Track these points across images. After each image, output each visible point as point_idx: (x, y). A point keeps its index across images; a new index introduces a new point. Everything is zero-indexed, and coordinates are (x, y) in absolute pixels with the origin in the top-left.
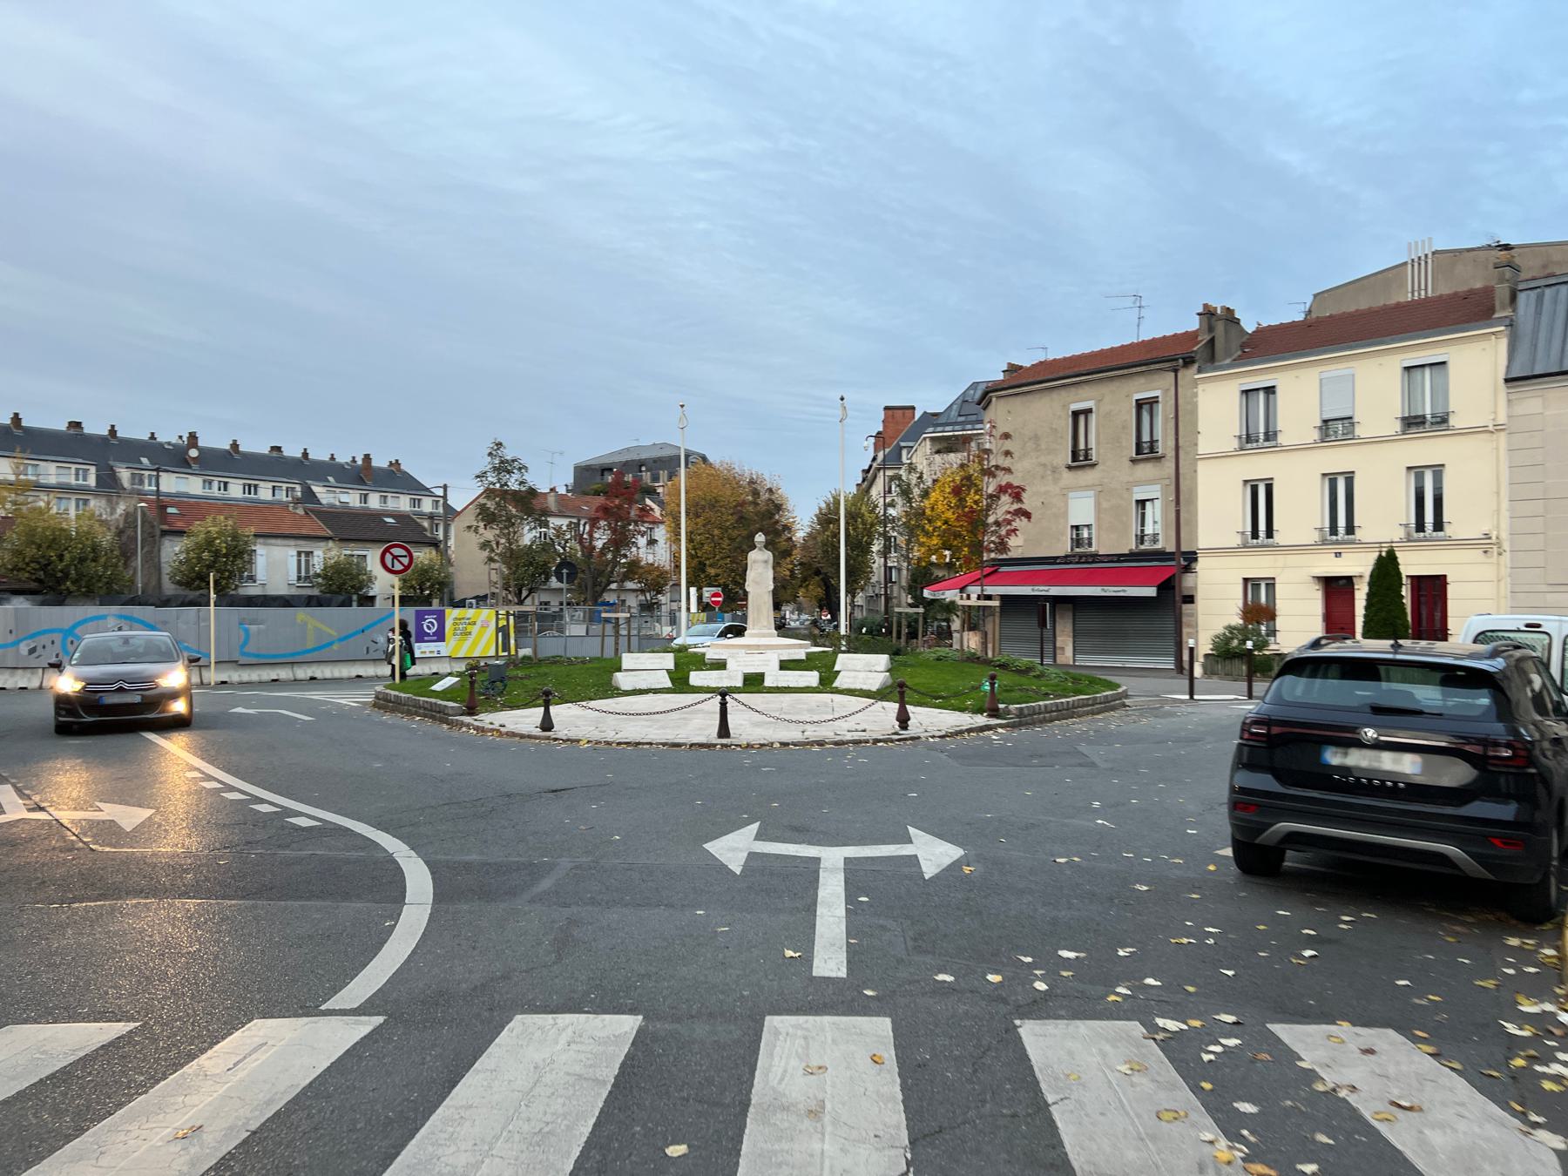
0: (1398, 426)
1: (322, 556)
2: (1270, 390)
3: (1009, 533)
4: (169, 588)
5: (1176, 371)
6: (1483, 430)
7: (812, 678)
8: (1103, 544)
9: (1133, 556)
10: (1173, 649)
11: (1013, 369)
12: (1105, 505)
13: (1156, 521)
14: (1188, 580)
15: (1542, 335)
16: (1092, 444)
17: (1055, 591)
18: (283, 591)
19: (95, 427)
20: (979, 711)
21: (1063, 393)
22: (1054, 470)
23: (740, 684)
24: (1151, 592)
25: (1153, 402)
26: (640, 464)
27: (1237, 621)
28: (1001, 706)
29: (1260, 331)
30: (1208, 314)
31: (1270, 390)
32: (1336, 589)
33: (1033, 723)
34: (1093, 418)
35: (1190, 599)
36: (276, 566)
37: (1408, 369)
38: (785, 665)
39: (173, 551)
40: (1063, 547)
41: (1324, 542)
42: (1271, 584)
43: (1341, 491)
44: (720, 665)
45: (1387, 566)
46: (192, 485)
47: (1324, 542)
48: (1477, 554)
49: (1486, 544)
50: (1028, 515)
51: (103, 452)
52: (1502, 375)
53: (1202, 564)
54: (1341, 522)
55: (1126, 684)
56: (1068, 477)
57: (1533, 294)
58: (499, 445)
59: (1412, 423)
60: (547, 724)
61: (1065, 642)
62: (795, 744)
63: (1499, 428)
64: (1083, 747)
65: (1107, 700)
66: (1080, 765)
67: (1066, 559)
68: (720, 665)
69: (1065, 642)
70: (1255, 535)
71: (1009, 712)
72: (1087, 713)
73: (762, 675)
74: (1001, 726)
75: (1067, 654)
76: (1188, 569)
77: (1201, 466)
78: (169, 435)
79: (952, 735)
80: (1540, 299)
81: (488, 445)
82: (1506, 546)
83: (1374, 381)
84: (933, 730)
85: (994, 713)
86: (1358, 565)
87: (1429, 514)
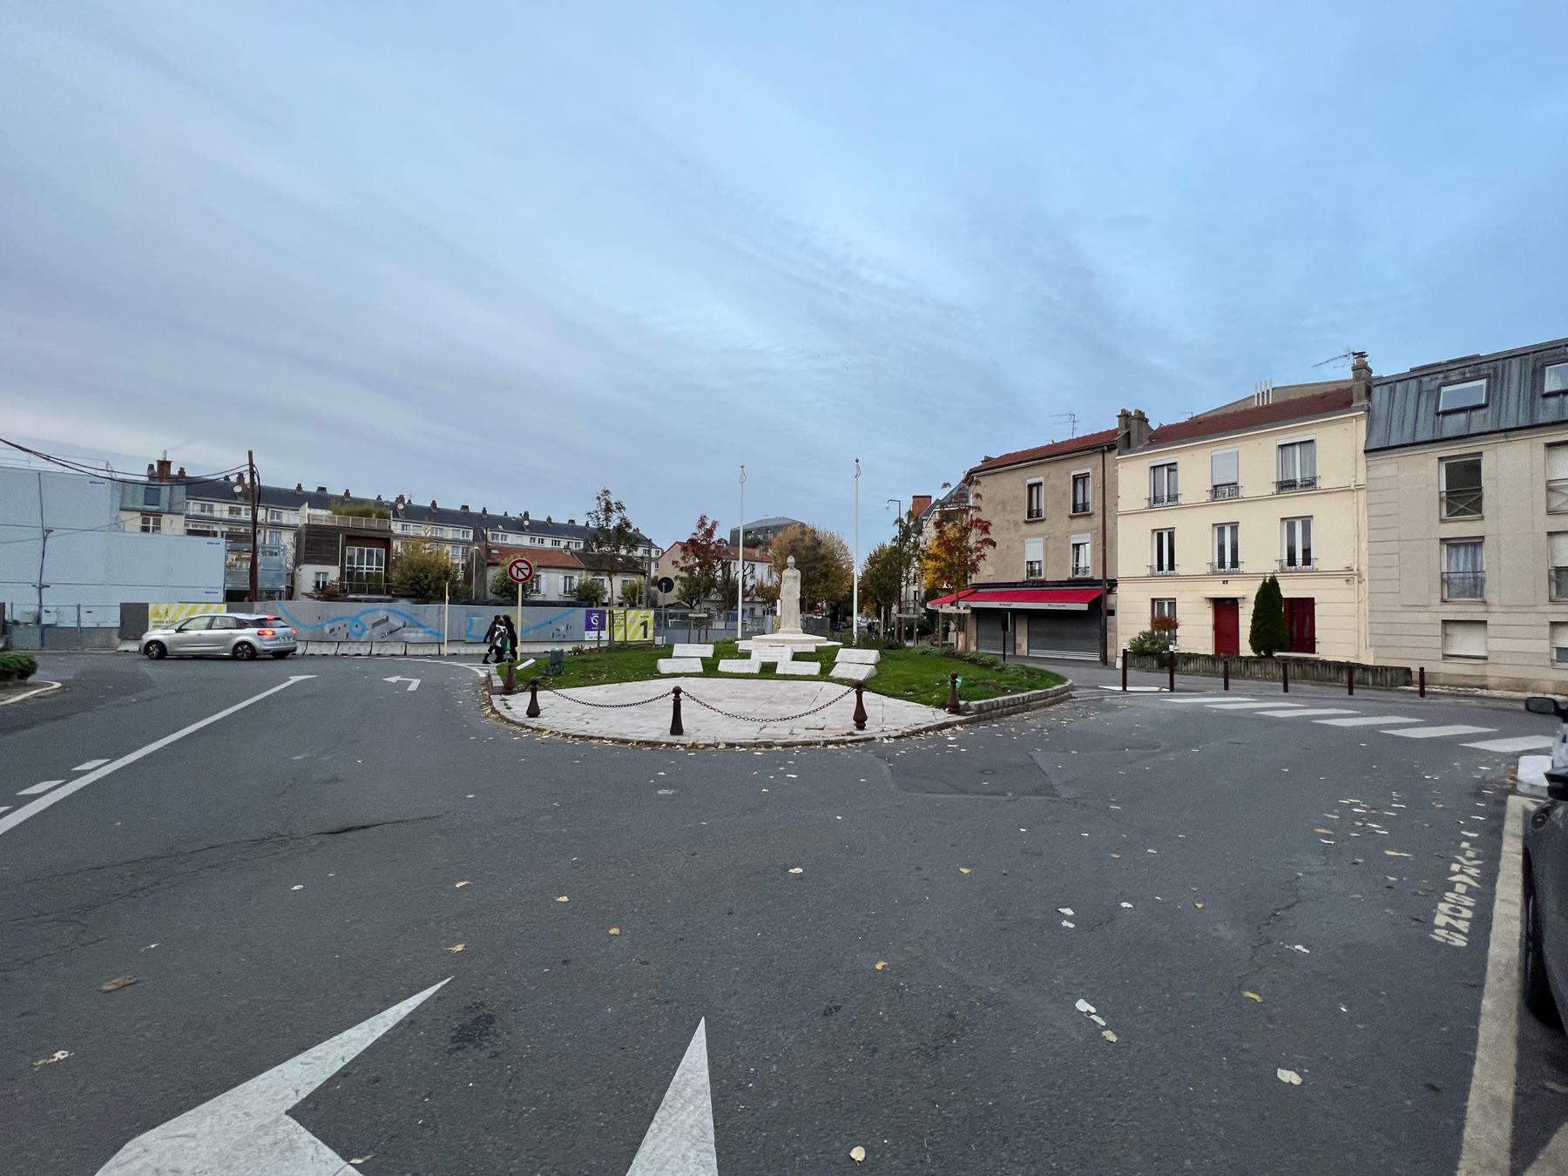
0: (1274, 489)
1: (578, 578)
2: (1172, 467)
3: (978, 558)
4: (490, 596)
5: (1103, 452)
6: (1347, 490)
7: (814, 668)
8: (1048, 575)
9: (1070, 582)
10: (1097, 643)
11: (988, 459)
12: (1051, 547)
13: (1087, 558)
14: (1111, 599)
15: (1395, 418)
16: (1042, 506)
17: (1015, 605)
18: (556, 599)
19: (475, 509)
20: (942, 706)
21: (1022, 472)
22: (1016, 524)
23: (756, 671)
24: (1084, 607)
25: (1085, 477)
26: (767, 529)
27: (1148, 628)
28: (962, 703)
29: (1162, 429)
30: (1125, 416)
31: (1172, 467)
32: (1225, 609)
33: (991, 718)
34: (1043, 489)
35: (1112, 613)
36: (552, 584)
37: (1282, 447)
38: (797, 657)
39: (492, 574)
40: (1021, 576)
41: (1214, 573)
42: (1172, 603)
43: (1227, 532)
44: (746, 655)
45: (1269, 590)
46: (525, 541)
47: (1214, 573)
48: (1341, 583)
49: (1349, 575)
50: (994, 544)
51: (480, 523)
52: (1361, 449)
53: (1121, 589)
54: (1228, 561)
55: (1072, 676)
56: (1025, 529)
57: (1386, 388)
58: (607, 492)
59: (1285, 485)
60: (534, 711)
61: (1022, 641)
62: (741, 746)
63: (1358, 488)
64: (1039, 756)
65: (1057, 693)
66: (1037, 792)
67: (1023, 584)
68: (746, 655)
69: (1022, 641)
70: (1160, 567)
71: (969, 709)
72: (1041, 706)
73: (775, 664)
74: (960, 723)
75: (1023, 648)
76: (1110, 591)
77: (1120, 520)
78: (514, 514)
79: (909, 735)
80: (1392, 391)
81: (696, 521)
82: (1365, 576)
83: (1255, 458)
84: (891, 729)
85: (955, 709)
86: (1246, 591)
87: (1299, 557)
